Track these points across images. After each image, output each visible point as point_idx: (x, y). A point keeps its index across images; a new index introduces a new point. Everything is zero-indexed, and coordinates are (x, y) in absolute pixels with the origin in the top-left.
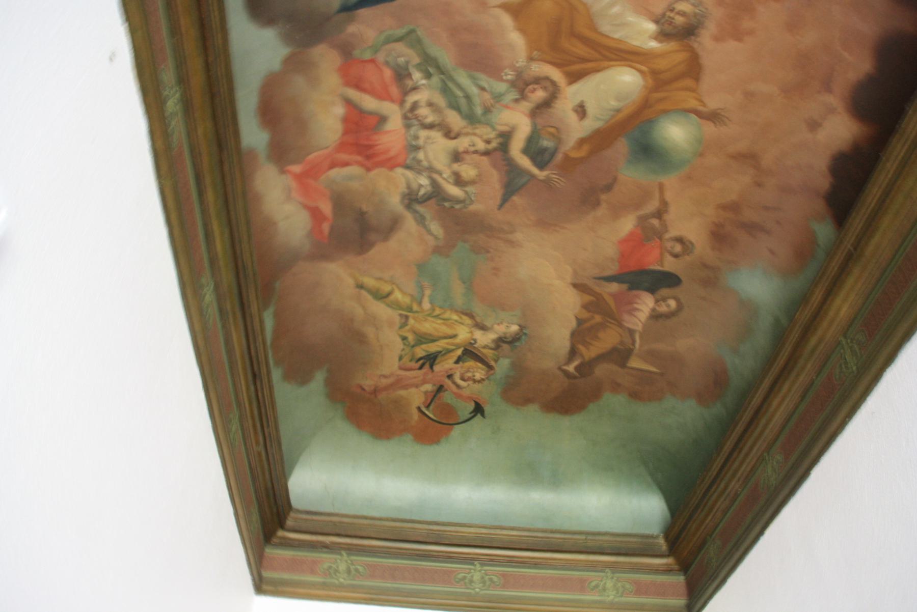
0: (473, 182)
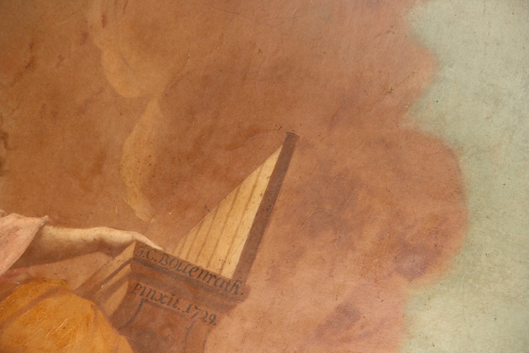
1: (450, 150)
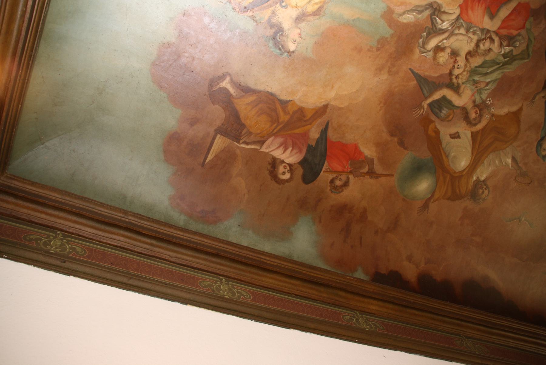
0: (435, 58)
1: (166, 161)
